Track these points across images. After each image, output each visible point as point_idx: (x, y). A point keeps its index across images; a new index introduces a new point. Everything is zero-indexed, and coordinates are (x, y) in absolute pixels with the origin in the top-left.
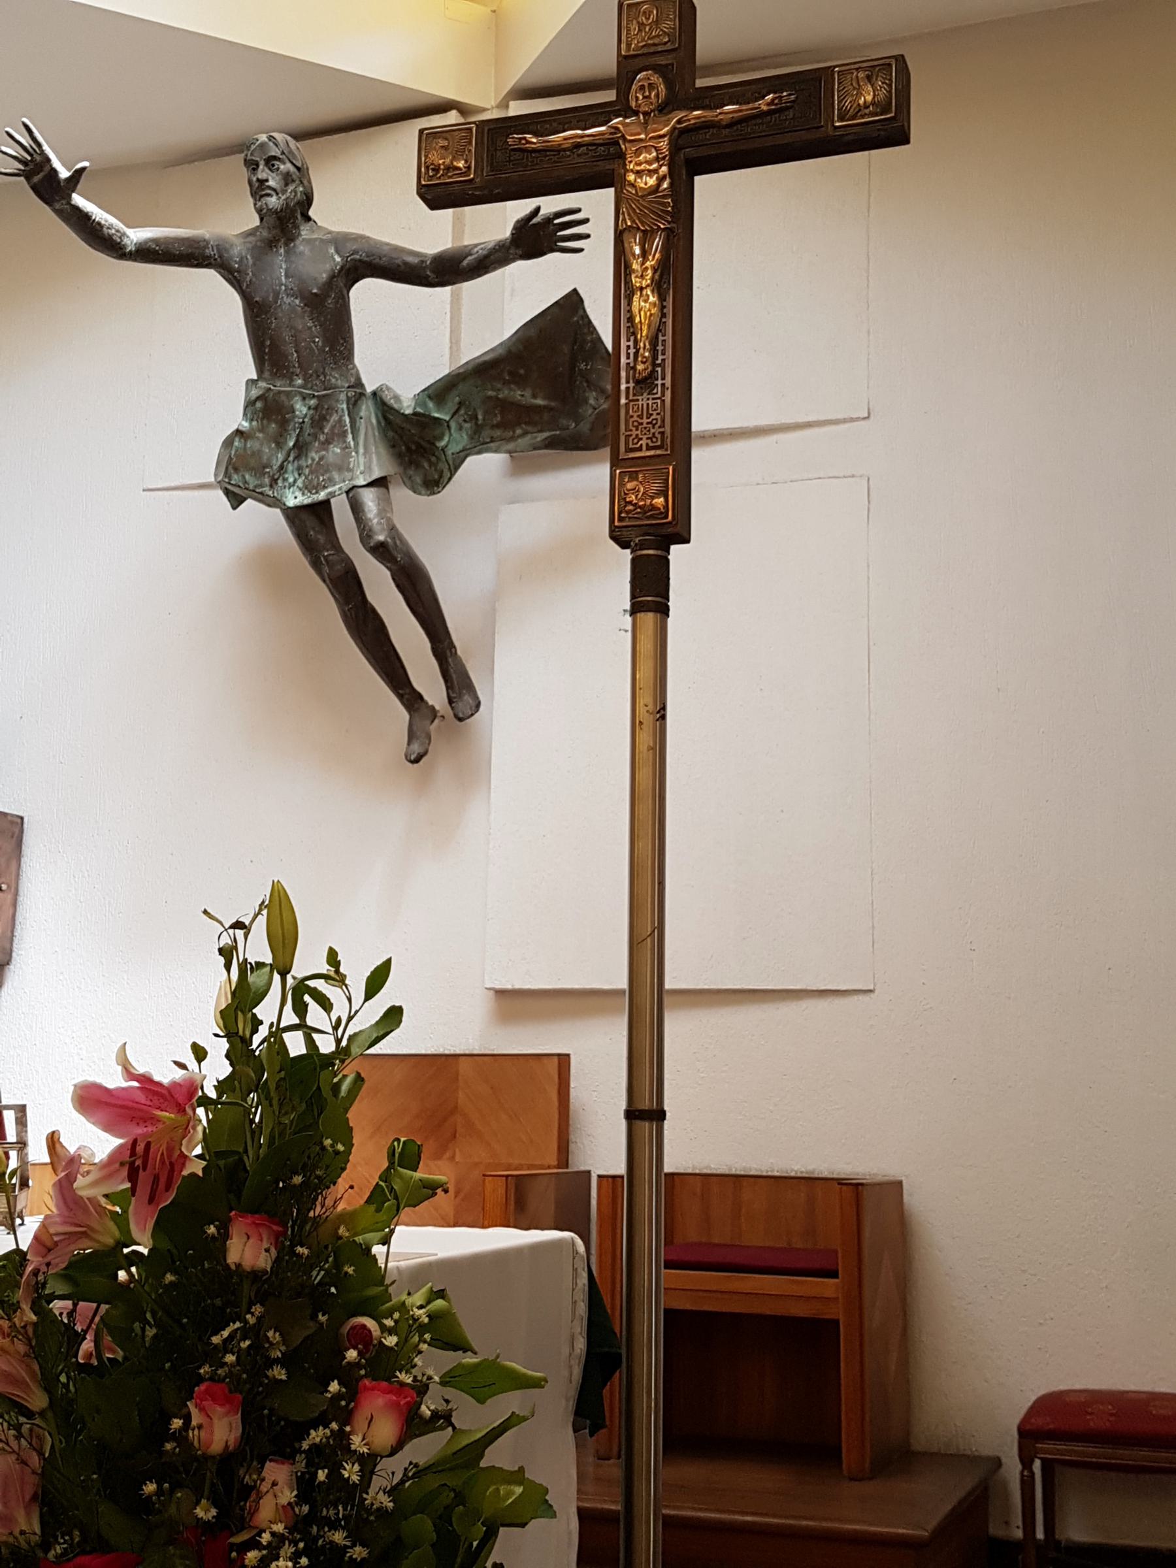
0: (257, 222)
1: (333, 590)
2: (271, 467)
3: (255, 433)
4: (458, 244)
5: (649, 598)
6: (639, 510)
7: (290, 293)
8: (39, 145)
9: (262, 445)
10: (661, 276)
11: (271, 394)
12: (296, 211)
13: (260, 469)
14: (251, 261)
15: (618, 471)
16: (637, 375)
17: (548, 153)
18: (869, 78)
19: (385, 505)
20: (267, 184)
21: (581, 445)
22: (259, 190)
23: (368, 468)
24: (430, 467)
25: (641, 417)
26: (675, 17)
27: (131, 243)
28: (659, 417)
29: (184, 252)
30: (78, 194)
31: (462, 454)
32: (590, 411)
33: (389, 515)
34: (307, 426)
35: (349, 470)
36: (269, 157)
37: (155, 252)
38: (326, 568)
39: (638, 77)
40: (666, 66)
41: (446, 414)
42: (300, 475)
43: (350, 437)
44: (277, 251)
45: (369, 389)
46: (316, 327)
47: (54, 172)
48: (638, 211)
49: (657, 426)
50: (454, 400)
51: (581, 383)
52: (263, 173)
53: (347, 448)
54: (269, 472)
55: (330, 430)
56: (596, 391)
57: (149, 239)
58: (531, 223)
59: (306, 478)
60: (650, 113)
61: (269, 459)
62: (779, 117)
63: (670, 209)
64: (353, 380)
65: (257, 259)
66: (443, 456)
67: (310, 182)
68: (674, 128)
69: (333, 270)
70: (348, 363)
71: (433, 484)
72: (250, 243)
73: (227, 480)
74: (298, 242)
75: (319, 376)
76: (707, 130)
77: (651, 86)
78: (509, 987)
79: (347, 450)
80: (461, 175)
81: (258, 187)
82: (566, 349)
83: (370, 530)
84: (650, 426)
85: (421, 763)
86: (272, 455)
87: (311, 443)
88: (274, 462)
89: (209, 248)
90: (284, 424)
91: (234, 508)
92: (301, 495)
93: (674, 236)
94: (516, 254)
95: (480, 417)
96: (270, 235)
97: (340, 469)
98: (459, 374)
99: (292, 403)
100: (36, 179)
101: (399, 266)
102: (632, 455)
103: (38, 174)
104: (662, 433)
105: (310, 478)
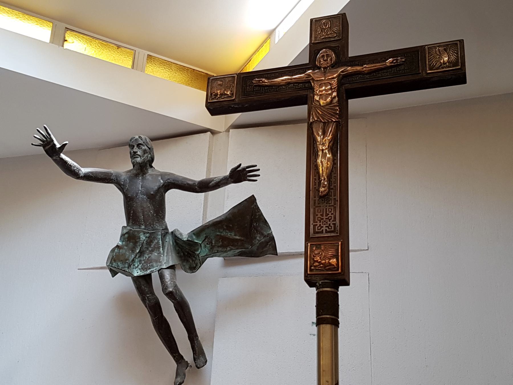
0: (132, 168)
2: (129, 260)
3: (124, 247)
4: (208, 177)
5: (328, 316)
6: (322, 265)
7: (142, 193)
8: (49, 135)
10: (333, 144)
12: (147, 164)
16: (320, 194)
17: (273, 87)
18: (445, 50)
19: (173, 276)
20: (137, 153)
21: (253, 255)
22: (134, 155)
23: (168, 261)
24: (192, 261)
25: (322, 215)
26: (340, 26)
28: (332, 216)
32: (257, 242)
33: (174, 280)
34: (145, 244)
35: (160, 262)
36: (138, 144)
39: (320, 52)
42: (140, 263)
43: (161, 249)
44: (139, 178)
45: (170, 231)
46: (151, 206)
47: (55, 145)
48: (320, 113)
49: (331, 221)
50: (203, 237)
51: (254, 231)
52: (136, 149)
53: (160, 253)
54: (128, 262)
55: (154, 246)
58: (237, 170)
59: (143, 264)
60: (327, 68)
62: (396, 69)
63: (338, 112)
64: (164, 227)
66: (198, 258)
67: (153, 153)
68: (339, 75)
69: (159, 185)
70: (163, 220)
71: (193, 269)
72: (129, 175)
73: (111, 265)
74: (147, 175)
75: (151, 225)
76: (357, 76)
77: (328, 56)
79: (160, 254)
80: (229, 97)
81: (133, 154)
82: (248, 217)
83: (167, 286)
84: (328, 220)
87: (145, 251)
89: (112, 176)
90: (135, 243)
91: (113, 277)
92: (140, 272)
93: (340, 125)
95: (213, 243)
96: (137, 172)
99: (140, 235)
100: (47, 147)
101: (185, 184)
102: (317, 235)
103: (49, 145)
104: (334, 224)
105: (144, 265)
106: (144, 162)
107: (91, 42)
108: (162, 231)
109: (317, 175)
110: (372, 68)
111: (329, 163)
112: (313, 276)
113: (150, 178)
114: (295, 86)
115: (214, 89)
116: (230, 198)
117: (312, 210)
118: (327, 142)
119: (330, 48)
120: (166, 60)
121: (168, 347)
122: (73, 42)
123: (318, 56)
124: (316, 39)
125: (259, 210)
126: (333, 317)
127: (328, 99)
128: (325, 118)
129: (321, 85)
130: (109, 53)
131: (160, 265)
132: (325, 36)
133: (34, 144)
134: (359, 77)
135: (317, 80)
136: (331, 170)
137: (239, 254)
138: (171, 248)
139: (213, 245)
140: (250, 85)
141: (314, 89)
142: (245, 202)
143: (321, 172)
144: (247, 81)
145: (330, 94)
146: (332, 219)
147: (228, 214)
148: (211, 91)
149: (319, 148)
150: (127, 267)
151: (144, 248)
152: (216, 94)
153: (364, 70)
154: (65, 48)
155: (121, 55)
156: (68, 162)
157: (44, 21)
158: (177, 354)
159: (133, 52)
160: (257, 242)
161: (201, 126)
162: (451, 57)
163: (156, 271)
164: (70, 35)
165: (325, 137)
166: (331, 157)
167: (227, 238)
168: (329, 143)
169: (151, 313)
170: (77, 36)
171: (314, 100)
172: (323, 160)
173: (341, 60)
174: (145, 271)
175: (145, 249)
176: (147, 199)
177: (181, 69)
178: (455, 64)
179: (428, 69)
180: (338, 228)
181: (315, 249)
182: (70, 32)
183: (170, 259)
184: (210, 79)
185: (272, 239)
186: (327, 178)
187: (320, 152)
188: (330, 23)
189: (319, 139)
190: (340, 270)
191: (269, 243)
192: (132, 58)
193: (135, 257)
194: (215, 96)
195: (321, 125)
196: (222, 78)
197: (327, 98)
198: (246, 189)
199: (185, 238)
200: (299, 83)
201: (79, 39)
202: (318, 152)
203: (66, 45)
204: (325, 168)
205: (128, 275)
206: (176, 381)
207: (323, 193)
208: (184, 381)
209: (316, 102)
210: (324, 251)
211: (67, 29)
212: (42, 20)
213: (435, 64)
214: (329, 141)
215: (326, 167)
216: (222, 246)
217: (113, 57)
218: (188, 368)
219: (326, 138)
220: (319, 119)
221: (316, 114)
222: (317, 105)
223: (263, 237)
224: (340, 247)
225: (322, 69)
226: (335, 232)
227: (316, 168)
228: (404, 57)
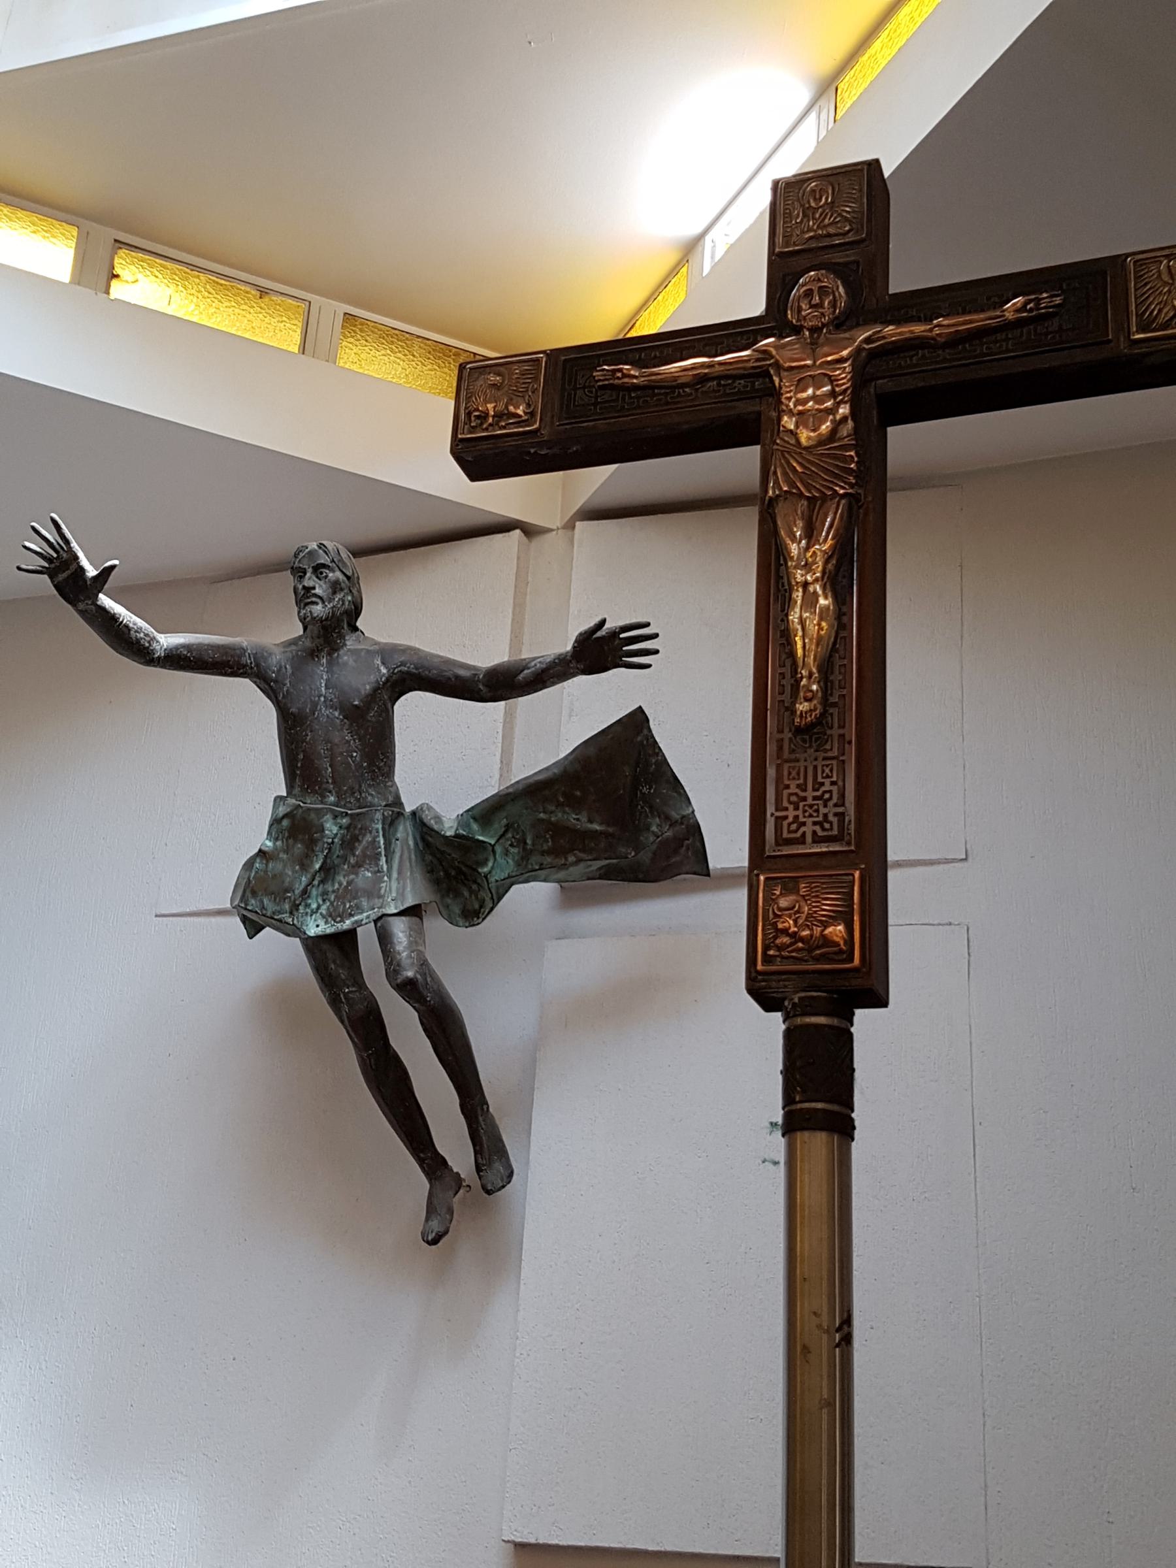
0: (301, 633)
2: (293, 891)
3: (278, 854)
4: (514, 658)
5: (820, 1105)
6: (800, 945)
8: (67, 542)
9: (285, 866)
10: (838, 567)
11: (300, 810)
13: (280, 894)
14: (289, 670)
15: (762, 878)
16: (797, 720)
19: (417, 937)
20: (313, 592)
22: (304, 597)
23: (401, 895)
26: (861, 197)
27: (161, 648)
28: (835, 789)
29: (218, 660)
32: (652, 839)
33: (420, 948)
34: (337, 846)
36: (318, 565)
39: (801, 281)
40: (846, 264)
41: (491, 837)
42: (324, 901)
43: (384, 859)
45: (408, 809)
46: (354, 740)
47: (82, 570)
48: (799, 469)
49: (831, 804)
51: (642, 808)
52: (310, 580)
53: (379, 871)
54: (290, 897)
57: (181, 645)
59: (332, 903)
60: (822, 329)
61: (291, 883)
62: (1035, 330)
64: (391, 799)
67: (359, 591)
68: (859, 350)
69: (377, 681)
70: (387, 780)
71: (473, 915)
72: (291, 652)
74: (341, 652)
76: (914, 353)
77: (823, 291)
78: (533, 1541)
81: (304, 594)
83: (399, 965)
85: (440, 1244)
87: (338, 866)
88: (297, 886)
89: (245, 656)
90: (311, 844)
91: (251, 938)
93: (860, 507)
95: (529, 842)
99: (321, 820)
100: (61, 577)
101: (449, 679)
103: (64, 572)
104: (841, 816)
105: (335, 904)
107: (187, 279)
109: (788, 663)
110: (960, 328)
111: (824, 624)
112: (773, 977)
113: (351, 660)
115: (476, 399)
116: (577, 716)
117: (771, 772)
118: (818, 559)
120: (396, 329)
121: (405, 1133)
122: (137, 281)
123: (793, 292)
125: (657, 751)
126: (835, 1108)
127: (824, 427)
128: (814, 484)
130: (237, 311)
131: (379, 905)
132: (815, 231)
133: (24, 567)
134: (920, 355)
135: (792, 368)
136: (830, 646)
137: (602, 871)
139: (529, 847)
143: (800, 652)
144: (576, 374)
145: (831, 409)
146: (835, 800)
147: (571, 763)
148: (466, 404)
150: (288, 910)
151: (335, 857)
153: (934, 333)
154: (112, 296)
156: (119, 618)
157: (54, 221)
160: (652, 839)
163: (367, 921)
164: (128, 260)
166: (831, 608)
168: (826, 562)
170: (148, 264)
171: (781, 428)
172: (808, 614)
173: (863, 306)
174: (337, 923)
175: (339, 859)
176: (342, 721)
177: (440, 352)
179: (1135, 329)
180: (852, 826)
181: (781, 894)
182: (127, 251)
183: (409, 889)
184: (464, 367)
185: (695, 830)
186: (819, 672)
187: (797, 591)
188: (830, 192)
189: (794, 549)
191: (687, 842)
192: (300, 324)
194: (479, 422)
196: (501, 367)
198: (622, 689)
199: (449, 828)
200: (735, 377)
201: (150, 271)
203: (118, 290)
204: (811, 640)
206: (427, 1229)
207: (806, 717)
208: (451, 1230)
210: (809, 900)
211: (117, 245)
212: (49, 219)
213: (1155, 312)
214: (826, 556)
215: (815, 636)
216: (554, 852)
217: (246, 322)
219: (817, 547)
220: (794, 488)
221: (785, 474)
222: (788, 446)
223: (669, 823)
224: (856, 889)
225: (807, 333)
227: (783, 641)
228: (1060, 292)
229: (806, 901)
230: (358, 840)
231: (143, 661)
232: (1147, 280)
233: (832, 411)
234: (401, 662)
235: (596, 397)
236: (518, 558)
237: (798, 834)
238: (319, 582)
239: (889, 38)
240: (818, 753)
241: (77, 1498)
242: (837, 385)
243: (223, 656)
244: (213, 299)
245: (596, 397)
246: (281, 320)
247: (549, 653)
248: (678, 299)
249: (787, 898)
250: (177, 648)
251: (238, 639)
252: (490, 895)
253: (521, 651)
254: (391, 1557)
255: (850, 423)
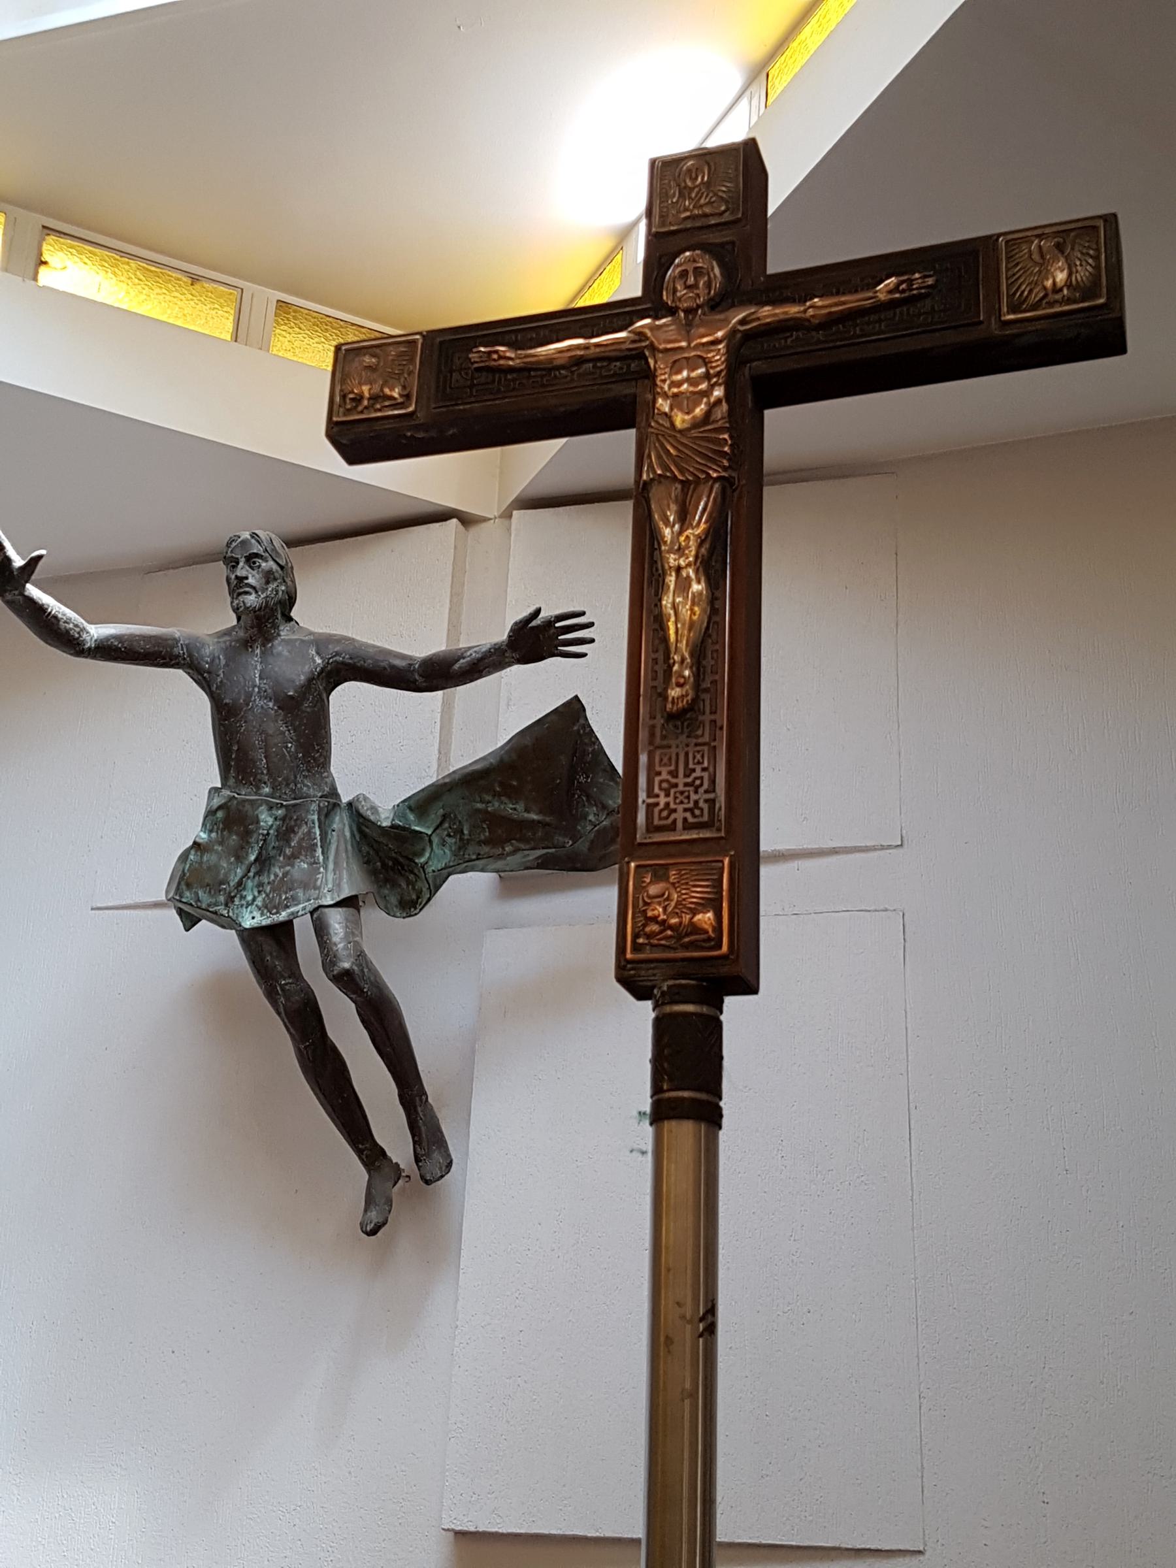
0: (235, 622)
1: (288, 1024)
3: (213, 846)
5: (686, 1094)
6: (669, 932)
10: (711, 551)
11: (235, 802)
13: (215, 886)
14: (223, 662)
15: (633, 865)
16: (669, 706)
17: (532, 373)
18: (1060, 247)
19: (354, 927)
20: (246, 581)
22: (237, 587)
23: (338, 885)
24: (408, 885)
25: (674, 774)
26: (737, 176)
27: (91, 639)
28: (706, 775)
30: (33, 585)
31: (446, 871)
32: (589, 828)
33: (357, 939)
34: (272, 838)
36: (250, 554)
37: (117, 649)
38: (282, 999)
40: (722, 245)
41: (428, 827)
42: (259, 892)
43: (319, 850)
44: (253, 651)
45: (345, 799)
46: (289, 731)
47: (8, 560)
49: (701, 790)
51: (579, 797)
52: (242, 570)
53: (315, 863)
55: (297, 843)
56: (596, 805)
58: (530, 625)
59: (267, 895)
60: (696, 310)
61: (226, 875)
62: (908, 310)
63: (726, 449)
65: (228, 659)
67: (293, 581)
68: (734, 332)
70: (322, 771)
71: (410, 905)
72: (225, 642)
74: (276, 642)
75: (288, 785)
76: (788, 334)
77: (698, 272)
78: (472, 1529)
82: (564, 760)
83: (335, 957)
84: (691, 789)
85: (379, 1234)
86: (230, 870)
88: (232, 877)
90: (246, 835)
91: (187, 930)
92: (259, 915)
93: (734, 491)
94: (513, 658)
95: (466, 832)
97: (306, 886)
98: (445, 784)
99: (256, 813)
102: (658, 838)
105: (271, 896)
106: (266, 606)
107: (116, 266)
108: (320, 802)
109: (661, 648)
111: (696, 609)
112: (643, 965)
114: (598, 371)
116: (514, 705)
117: (643, 759)
118: (691, 543)
119: (706, 248)
120: (330, 317)
122: (65, 268)
124: (664, 221)
125: (593, 739)
126: (703, 1096)
129: (677, 363)
130: (168, 298)
131: (315, 896)
132: (691, 211)
134: (794, 337)
135: (667, 350)
136: (703, 630)
138: (346, 848)
139: (466, 837)
140: (463, 366)
141: (654, 377)
142: (553, 717)
147: (507, 752)
149: (668, 563)
151: (270, 848)
152: (358, 398)
155: (200, 300)
156: (47, 609)
158: (367, 1146)
159: (236, 293)
161: (432, 503)
162: (1077, 272)
163: (303, 912)
165: (685, 528)
166: (704, 592)
167: (503, 817)
168: (700, 546)
169: (292, 1030)
171: (656, 411)
174: (273, 914)
176: (276, 711)
178: (1089, 291)
183: (345, 880)
186: (692, 655)
187: (671, 575)
189: (667, 532)
190: (725, 948)
192: (232, 312)
193: (246, 875)
194: (354, 405)
195: (676, 488)
197: (698, 404)
200: (610, 359)
201: (80, 258)
202: (664, 574)
203: (45, 276)
204: (683, 625)
205: (226, 926)
209: (663, 420)
210: (678, 887)
211: (46, 231)
213: (1026, 293)
214: (699, 540)
217: (177, 309)
218: (400, 1181)
220: (667, 470)
221: (659, 457)
222: (663, 429)
223: (606, 812)
225: (682, 315)
226: (713, 826)
227: (656, 626)
228: (932, 273)
229: (676, 888)
230: (294, 832)
231: (72, 652)
232: (1017, 261)
233: (706, 393)
234: (336, 652)
235: (473, 378)
236: (455, 547)
237: (670, 821)
238: (251, 571)
239: (819, 23)
240: (689, 740)
241: (16, 1492)
242: (712, 367)
243: (155, 647)
244: (144, 286)
245: (473, 378)
246: (212, 307)
247: (484, 642)
248: (613, 286)
249: (657, 886)
250: (108, 638)
251: (170, 630)
252: (427, 886)
253: (459, 640)
254: (331, 1547)
255: (725, 406)
